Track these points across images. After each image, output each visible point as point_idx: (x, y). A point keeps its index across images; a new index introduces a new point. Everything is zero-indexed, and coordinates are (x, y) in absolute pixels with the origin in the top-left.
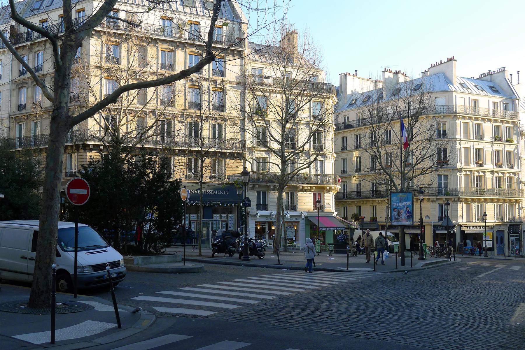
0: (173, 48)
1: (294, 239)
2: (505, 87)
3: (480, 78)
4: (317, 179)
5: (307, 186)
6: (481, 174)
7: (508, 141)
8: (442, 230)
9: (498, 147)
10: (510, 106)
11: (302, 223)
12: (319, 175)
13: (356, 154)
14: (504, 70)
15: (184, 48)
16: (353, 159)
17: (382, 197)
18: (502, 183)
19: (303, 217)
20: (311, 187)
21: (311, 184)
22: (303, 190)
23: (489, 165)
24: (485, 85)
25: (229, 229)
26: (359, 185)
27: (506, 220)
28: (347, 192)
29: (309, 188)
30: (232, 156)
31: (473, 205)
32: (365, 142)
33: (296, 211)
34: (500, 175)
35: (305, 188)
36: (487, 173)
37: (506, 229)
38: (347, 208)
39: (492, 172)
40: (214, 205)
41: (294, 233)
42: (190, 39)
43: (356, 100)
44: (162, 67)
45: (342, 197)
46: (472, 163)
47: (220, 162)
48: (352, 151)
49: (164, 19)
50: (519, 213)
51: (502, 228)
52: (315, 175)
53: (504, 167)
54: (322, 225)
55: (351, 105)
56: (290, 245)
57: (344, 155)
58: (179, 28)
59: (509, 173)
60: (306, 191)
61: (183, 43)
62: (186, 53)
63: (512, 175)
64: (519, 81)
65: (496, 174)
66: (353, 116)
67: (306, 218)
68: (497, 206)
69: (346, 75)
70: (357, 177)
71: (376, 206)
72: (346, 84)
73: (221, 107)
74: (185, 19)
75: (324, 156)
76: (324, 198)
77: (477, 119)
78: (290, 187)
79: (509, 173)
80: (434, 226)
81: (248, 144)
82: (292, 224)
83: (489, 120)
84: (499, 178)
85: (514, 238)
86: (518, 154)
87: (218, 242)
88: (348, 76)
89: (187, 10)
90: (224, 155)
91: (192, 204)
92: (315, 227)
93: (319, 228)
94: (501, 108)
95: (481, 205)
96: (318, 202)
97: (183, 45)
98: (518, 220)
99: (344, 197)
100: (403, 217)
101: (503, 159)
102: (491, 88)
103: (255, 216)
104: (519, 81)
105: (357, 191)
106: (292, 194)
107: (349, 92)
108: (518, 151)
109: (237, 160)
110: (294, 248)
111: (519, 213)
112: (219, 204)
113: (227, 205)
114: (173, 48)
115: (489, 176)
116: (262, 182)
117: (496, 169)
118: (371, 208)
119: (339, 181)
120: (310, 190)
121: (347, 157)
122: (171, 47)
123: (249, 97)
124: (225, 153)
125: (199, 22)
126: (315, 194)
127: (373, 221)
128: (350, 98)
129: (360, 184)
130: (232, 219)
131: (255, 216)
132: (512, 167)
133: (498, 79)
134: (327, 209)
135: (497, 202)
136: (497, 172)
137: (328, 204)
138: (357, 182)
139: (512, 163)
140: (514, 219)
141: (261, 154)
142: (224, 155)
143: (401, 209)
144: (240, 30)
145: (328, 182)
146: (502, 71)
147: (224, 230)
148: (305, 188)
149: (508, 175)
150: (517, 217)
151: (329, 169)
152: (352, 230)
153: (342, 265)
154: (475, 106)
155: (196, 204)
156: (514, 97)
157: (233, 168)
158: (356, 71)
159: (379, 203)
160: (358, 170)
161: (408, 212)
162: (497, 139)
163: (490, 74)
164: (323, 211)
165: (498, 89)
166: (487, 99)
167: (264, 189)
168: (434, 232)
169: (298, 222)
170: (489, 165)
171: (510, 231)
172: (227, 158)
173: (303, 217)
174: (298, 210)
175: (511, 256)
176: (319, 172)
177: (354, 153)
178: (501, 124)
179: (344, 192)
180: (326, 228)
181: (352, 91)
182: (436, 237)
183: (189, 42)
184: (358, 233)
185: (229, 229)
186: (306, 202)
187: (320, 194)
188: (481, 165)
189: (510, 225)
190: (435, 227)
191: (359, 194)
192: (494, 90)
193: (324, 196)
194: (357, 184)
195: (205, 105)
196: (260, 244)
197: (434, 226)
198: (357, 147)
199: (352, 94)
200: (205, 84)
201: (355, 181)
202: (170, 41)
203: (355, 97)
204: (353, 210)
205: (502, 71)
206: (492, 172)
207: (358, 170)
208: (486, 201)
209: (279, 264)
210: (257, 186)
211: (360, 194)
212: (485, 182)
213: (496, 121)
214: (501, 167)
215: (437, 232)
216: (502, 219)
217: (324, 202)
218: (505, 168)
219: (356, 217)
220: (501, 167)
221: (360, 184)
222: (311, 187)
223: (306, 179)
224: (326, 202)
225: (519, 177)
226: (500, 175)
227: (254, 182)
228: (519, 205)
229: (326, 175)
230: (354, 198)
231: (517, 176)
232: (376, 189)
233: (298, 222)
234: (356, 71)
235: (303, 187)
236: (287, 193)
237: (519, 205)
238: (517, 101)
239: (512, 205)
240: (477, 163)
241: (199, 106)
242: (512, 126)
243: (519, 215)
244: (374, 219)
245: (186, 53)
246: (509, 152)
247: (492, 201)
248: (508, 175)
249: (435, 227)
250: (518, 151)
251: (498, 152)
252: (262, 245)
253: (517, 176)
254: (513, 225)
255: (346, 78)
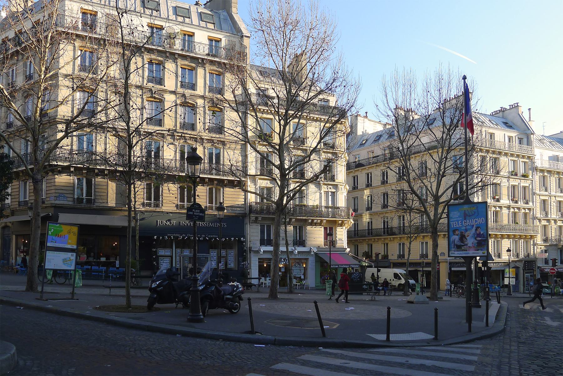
0: (162, 59)
1: (302, 277)
2: (519, 123)
3: (492, 115)
4: (328, 211)
5: (317, 220)
6: (498, 209)
7: (524, 176)
8: (462, 267)
9: (513, 182)
10: (525, 140)
11: (312, 260)
12: (331, 207)
13: (367, 192)
14: (518, 106)
15: (175, 61)
16: (365, 197)
17: (393, 234)
18: (517, 219)
19: (312, 253)
20: (322, 221)
21: (321, 217)
22: (312, 224)
23: (505, 201)
24: (500, 121)
25: (229, 266)
26: (370, 223)
27: (522, 256)
28: (358, 230)
29: (319, 221)
30: (231, 184)
31: (490, 241)
32: (377, 180)
33: (304, 246)
34: (516, 210)
35: (315, 221)
36: (504, 208)
37: (521, 265)
38: (357, 246)
39: (509, 207)
40: (210, 239)
41: (303, 271)
42: (182, 50)
43: (367, 140)
44: (149, 81)
45: (353, 236)
46: (489, 198)
47: (218, 191)
48: (363, 190)
49: (151, 27)
50: (534, 250)
51: (518, 264)
52: (326, 207)
53: (519, 203)
54: (335, 262)
55: (362, 145)
56: (298, 284)
57: (355, 194)
58: (171, 37)
59: (524, 209)
60: (316, 224)
61: (174, 54)
62: (177, 65)
63: (527, 211)
64: (530, 118)
65: (512, 210)
66: (363, 155)
67: (316, 254)
68: (513, 242)
69: (357, 116)
70: (368, 216)
71: (387, 244)
72: (356, 124)
73: (220, 129)
74: (177, 29)
75: (336, 187)
76: (336, 234)
77: (494, 152)
78: (297, 220)
79: (524, 209)
80: (450, 263)
81: (252, 171)
82: (299, 261)
83: (506, 154)
84: (515, 213)
85: (529, 274)
86: (532, 189)
87: (159, 286)
88: (359, 118)
89: (180, 19)
90: (222, 183)
91: (183, 238)
92: (325, 264)
93: (330, 265)
94: (516, 143)
95: (498, 241)
96: (329, 234)
97: (174, 56)
98: (533, 257)
99: (369, 234)
100: (470, 244)
101: (519, 194)
102: (505, 124)
103: (258, 252)
104: (530, 118)
105: (369, 229)
106: (301, 229)
107: (359, 133)
108: (532, 187)
109: (237, 190)
110: (302, 287)
111: (534, 250)
112: (215, 238)
113: (226, 239)
114: (162, 59)
115: (505, 211)
116: (267, 214)
117: (512, 204)
118: (383, 245)
119: (352, 214)
120: (320, 224)
121: (359, 196)
122: (159, 58)
123: (251, 121)
124: (223, 181)
125: (194, 33)
126: (325, 229)
127: (385, 259)
128: (361, 138)
129: (371, 222)
130: (231, 256)
131: (258, 252)
132: (527, 203)
133: (511, 116)
134: (339, 245)
135: (513, 238)
136: (513, 208)
137: (340, 240)
138: (368, 220)
139: (527, 198)
140: (528, 255)
141: (264, 183)
142: (222, 183)
143: (466, 230)
144: (242, 44)
145: (340, 216)
146: (515, 107)
147: (169, 266)
148: (315, 221)
149: (523, 211)
150: (532, 252)
151: (342, 201)
152: (363, 268)
153: (373, 326)
154: (491, 138)
155: (189, 238)
156: (528, 132)
157: (232, 198)
158: (366, 113)
159: (391, 241)
160: (369, 209)
161: (479, 235)
162: (514, 174)
163: (503, 110)
164: (334, 247)
165: (511, 124)
166: (503, 133)
167: (268, 222)
168: (450, 269)
169: (307, 259)
170: (505, 201)
171: (525, 268)
172: (226, 186)
173: (312, 253)
174: (307, 246)
175: (526, 293)
176: (330, 204)
177: (365, 191)
178: (516, 159)
179: (355, 231)
180: (339, 265)
181: (363, 132)
182: (452, 275)
183: (180, 52)
184: (370, 272)
185: (229, 266)
186: (316, 236)
187: (331, 229)
188: (498, 200)
189: (525, 262)
190: (451, 264)
191: (371, 232)
192: (508, 125)
193: (336, 230)
194: (369, 223)
195: (199, 126)
196: (230, 289)
197: (450, 263)
198: (369, 185)
199: (363, 135)
200: (200, 102)
201: (366, 218)
202: (159, 51)
203: (365, 138)
204: (364, 248)
205: (515, 107)
206: (509, 207)
207: (369, 209)
208: (502, 237)
209: (252, 332)
210: (260, 219)
211: (372, 232)
212: (502, 217)
213: (512, 155)
214: (516, 202)
215: (453, 269)
216: (518, 256)
217: (336, 237)
218: (521, 204)
219: (368, 255)
220: (516, 202)
221: (371, 222)
222: (322, 221)
223: (315, 212)
224: (338, 237)
225: (533, 213)
226: (516, 210)
227: (257, 214)
228: (534, 241)
229: (338, 208)
230: (365, 236)
231: (532, 212)
232: (372, 227)
233: (307, 259)
234: (366, 113)
235: (313, 220)
236: (295, 228)
237: (534, 241)
238: (532, 136)
239: (527, 242)
240: (494, 198)
241: (193, 127)
242: (527, 161)
243: (534, 252)
244: (386, 257)
245: (177, 65)
246: (525, 188)
247: (509, 237)
248: (523, 211)
249: (451, 264)
250: (532, 187)
251: (514, 187)
252: (234, 291)
253: (532, 212)
254: (528, 262)
255: (357, 119)
